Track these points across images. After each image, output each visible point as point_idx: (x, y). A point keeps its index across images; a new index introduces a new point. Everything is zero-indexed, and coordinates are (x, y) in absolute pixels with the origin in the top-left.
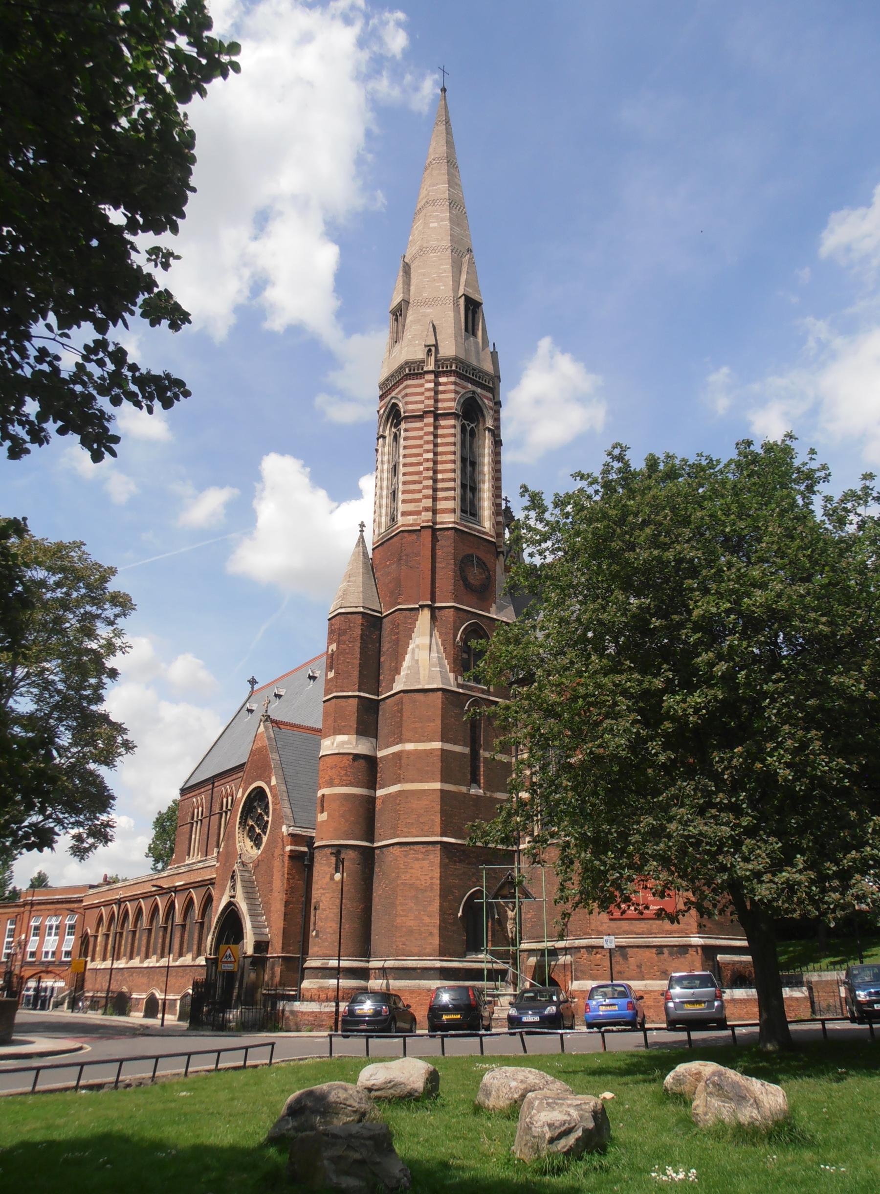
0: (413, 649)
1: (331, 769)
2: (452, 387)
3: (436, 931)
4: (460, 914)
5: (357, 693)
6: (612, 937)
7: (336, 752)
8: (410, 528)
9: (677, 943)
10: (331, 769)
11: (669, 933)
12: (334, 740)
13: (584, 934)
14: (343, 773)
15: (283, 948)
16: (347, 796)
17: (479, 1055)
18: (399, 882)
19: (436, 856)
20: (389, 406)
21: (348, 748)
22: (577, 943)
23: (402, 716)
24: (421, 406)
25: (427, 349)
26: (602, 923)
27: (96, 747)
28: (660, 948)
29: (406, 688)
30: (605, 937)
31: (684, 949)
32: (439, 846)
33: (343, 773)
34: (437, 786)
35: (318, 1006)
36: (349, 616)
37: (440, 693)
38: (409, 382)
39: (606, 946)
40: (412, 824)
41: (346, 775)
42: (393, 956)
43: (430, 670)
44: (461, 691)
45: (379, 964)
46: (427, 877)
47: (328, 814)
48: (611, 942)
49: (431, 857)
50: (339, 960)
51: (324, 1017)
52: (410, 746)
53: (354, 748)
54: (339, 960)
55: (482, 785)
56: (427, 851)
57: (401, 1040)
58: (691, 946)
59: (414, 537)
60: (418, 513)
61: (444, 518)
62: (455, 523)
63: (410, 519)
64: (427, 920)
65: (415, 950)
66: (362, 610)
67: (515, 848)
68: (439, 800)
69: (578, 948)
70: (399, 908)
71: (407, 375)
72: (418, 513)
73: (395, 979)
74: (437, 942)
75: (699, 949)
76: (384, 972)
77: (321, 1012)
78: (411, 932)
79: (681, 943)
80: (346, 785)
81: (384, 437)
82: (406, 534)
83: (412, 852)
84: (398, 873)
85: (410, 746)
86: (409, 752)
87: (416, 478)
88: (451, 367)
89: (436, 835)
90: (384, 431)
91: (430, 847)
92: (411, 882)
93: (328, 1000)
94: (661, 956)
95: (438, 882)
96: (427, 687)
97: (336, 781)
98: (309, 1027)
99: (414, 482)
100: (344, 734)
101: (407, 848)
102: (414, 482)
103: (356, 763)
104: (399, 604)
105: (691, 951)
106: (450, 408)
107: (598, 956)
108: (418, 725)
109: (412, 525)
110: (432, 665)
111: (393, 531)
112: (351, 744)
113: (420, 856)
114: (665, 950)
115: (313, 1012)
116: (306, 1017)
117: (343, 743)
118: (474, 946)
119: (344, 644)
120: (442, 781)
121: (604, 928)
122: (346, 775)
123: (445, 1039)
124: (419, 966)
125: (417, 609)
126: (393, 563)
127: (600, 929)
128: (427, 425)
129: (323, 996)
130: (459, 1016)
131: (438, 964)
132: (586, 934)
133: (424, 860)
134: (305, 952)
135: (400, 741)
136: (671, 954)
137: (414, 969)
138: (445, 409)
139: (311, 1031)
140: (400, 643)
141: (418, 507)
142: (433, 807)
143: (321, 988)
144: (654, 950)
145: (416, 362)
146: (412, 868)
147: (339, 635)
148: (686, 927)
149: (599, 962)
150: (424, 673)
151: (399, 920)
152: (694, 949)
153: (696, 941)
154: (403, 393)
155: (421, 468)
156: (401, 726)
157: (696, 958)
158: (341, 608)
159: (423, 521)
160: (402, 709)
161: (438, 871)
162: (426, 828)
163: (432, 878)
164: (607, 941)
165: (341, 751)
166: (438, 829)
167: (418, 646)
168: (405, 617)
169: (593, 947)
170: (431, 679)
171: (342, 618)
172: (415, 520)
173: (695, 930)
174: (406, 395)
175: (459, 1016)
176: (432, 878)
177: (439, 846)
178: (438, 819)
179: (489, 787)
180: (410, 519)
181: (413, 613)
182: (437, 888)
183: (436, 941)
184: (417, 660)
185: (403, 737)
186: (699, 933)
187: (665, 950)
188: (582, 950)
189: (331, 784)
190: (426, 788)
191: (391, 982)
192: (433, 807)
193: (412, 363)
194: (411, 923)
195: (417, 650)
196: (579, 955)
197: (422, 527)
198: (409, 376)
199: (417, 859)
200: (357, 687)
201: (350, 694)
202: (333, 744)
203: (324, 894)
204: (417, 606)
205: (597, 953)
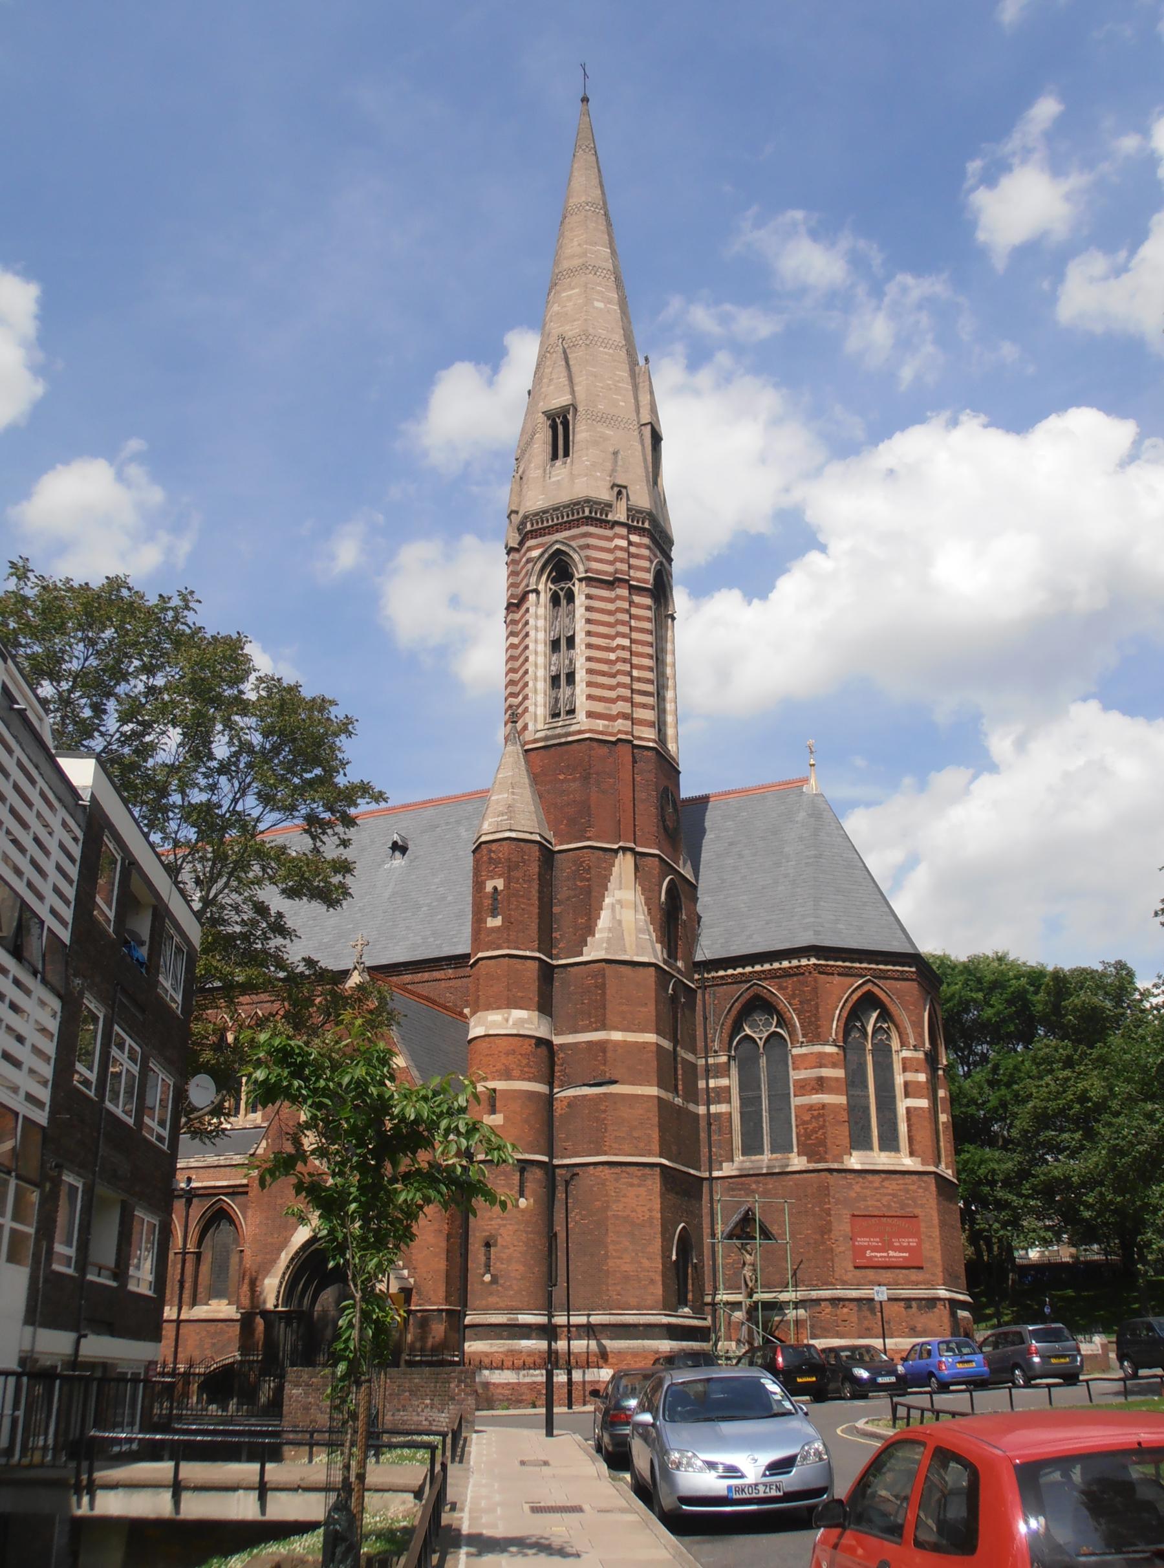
0: (613, 907)
1: (507, 1054)
2: (646, 552)
3: (658, 1278)
4: (674, 1257)
5: (537, 955)
6: (884, 1288)
7: (514, 1032)
8: (600, 737)
9: (926, 1296)
10: (507, 1054)
11: (915, 1284)
12: (509, 1014)
13: (823, 1284)
14: (525, 1062)
15: (447, 1298)
16: (531, 1095)
17: (1010, 1410)
18: (610, 1213)
19: (655, 1183)
20: (551, 552)
21: (530, 1029)
22: (814, 1294)
23: (604, 994)
24: (610, 569)
25: (616, 489)
26: (846, 1271)
27: (963, 1053)
28: (908, 1300)
29: (609, 957)
30: (876, 1288)
31: (933, 1302)
32: (658, 1169)
33: (525, 1062)
34: (653, 1091)
35: (515, 1376)
36: (522, 844)
37: (652, 969)
38: (592, 529)
39: (876, 1298)
40: (624, 1138)
41: (528, 1065)
42: (604, 1309)
43: (637, 937)
44: (665, 967)
45: (582, 1320)
46: (645, 1209)
47: (505, 1117)
48: (882, 1294)
49: (649, 1182)
50: (569, 1315)
51: (524, 1389)
52: (617, 1036)
53: (536, 1029)
54: (569, 1315)
55: (680, 1093)
56: (643, 1175)
57: (968, 1394)
58: (939, 1299)
59: (604, 750)
60: (611, 718)
61: (642, 732)
62: (654, 741)
63: (600, 724)
64: (646, 1263)
65: (633, 1301)
66: (538, 838)
67: (706, 1175)
68: (656, 1109)
69: (818, 1301)
70: (611, 1247)
71: (587, 518)
72: (611, 718)
73: (612, 1339)
74: (660, 1292)
75: (947, 1302)
76: (590, 1331)
77: (519, 1384)
78: (626, 1278)
79: (930, 1296)
80: (529, 1080)
81: (537, 592)
82: (595, 744)
83: (625, 1175)
84: (607, 1202)
85: (617, 1036)
86: (617, 1044)
87: (604, 667)
88: (583, 512)
89: (654, 1155)
90: (537, 583)
91: (647, 1170)
92: (625, 1214)
93: (535, 1366)
94: (909, 1310)
95: (659, 1215)
96: (636, 959)
97: (516, 1073)
98: (506, 1404)
99: (603, 674)
100: (521, 1008)
101: (618, 1170)
102: (603, 674)
103: (539, 1050)
104: (589, 839)
105: (939, 1305)
106: (645, 581)
107: (845, 1310)
108: (624, 1008)
109: (601, 733)
110: (639, 931)
111: (559, 736)
112: (532, 1023)
113: (636, 1181)
114: (914, 1304)
115: (508, 1384)
116: (499, 1390)
117: (521, 1022)
118: (683, 1302)
119: (517, 882)
120: (660, 1086)
121: (848, 1277)
122: (528, 1065)
123: (1052, 1389)
124: (641, 1322)
125: (616, 851)
126: (574, 780)
127: (845, 1278)
128: (618, 598)
129: (508, 1363)
130: (814, 1379)
131: (665, 1320)
132: (827, 1284)
133: (639, 1186)
134: (465, 1304)
135: (603, 1027)
136: (919, 1308)
137: (635, 1326)
138: (638, 580)
139: (508, 1408)
140: (594, 894)
141: (610, 709)
142: (649, 1119)
143: (512, 1351)
144: (902, 1304)
145: (600, 503)
146: (625, 1196)
147: (510, 869)
148: (932, 1278)
149: (846, 1318)
150: (630, 939)
151: (611, 1263)
152: (942, 1303)
153: (943, 1293)
154: (582, 541)
155: (612, 656)
156: (604, 1008)
157: (943, 1312)
158: (511, 830)
159: (619, 732)
160: (604, 984)
161: (659, 1201)
162: (642, 1145)
163: (650, 1210)
164: (878, 1293)
165: (522, 1032)
166: (656, 1147)
167: (619, 902)
168: (598, 858)
169: (840, 1300)
170: (640, 948)
171: (513, 845)
172: (604, 726)
173: (941, 1282)
174: (588, 546)
175: (814, 1379)
176: (650, 1210)
177: (658, 1169)
178: (655, 1135)
179: (685, 1099)
180: (600, 724)
181: (608, 855)
182: (658, 1223)
183: (658, 1290)
184: (620, 922)
185: (607, 1022)
186: (944, 1285)
187: (914, 1304)
188: (823, 1304)
189: (507, 1075)
190: (640, 1092)
191: (604, 1342)
192: (649, 1119)
193: (596, 503)
194: (626, 1267)
195: (618, 907)
196: (818, 1309)
197: (620, 740)
198: (589, 521)
199: (632, 1185)
200: (536, 945)
201: (528, 953)
202: (507, 1020)
203: (505, 1226)
204: (615, 846)
205: (844, 1306)
